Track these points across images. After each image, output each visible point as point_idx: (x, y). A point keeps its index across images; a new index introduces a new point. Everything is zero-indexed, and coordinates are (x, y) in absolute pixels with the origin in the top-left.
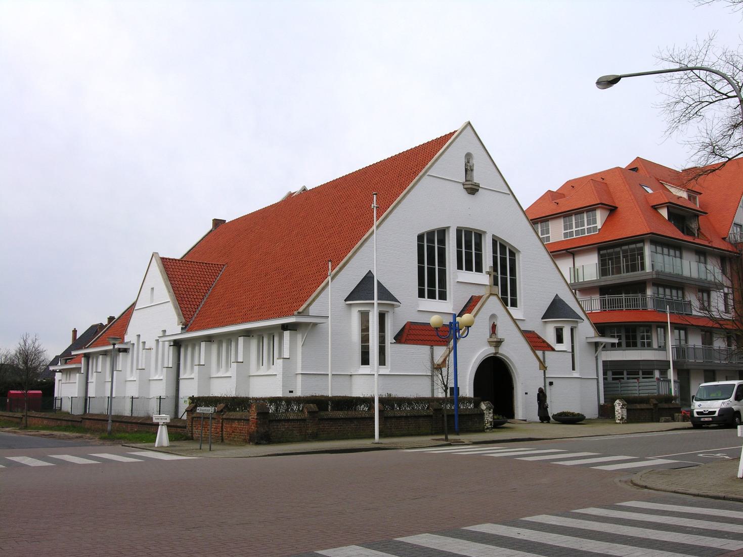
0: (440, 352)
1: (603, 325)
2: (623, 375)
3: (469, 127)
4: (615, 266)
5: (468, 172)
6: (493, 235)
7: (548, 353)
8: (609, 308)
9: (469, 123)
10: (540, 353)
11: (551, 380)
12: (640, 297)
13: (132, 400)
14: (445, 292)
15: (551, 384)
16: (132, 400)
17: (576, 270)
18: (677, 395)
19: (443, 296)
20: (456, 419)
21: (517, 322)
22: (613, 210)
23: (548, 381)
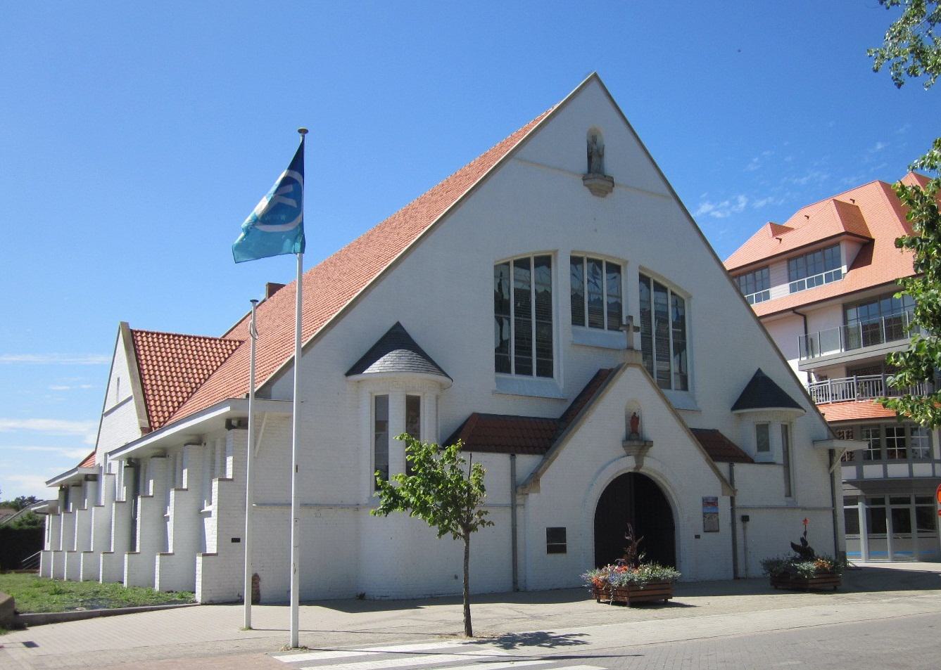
0: (526, 462)
1: (859, 423)
2: (893, 510)
3: (595, 83)
4: (869, 331)
5: (594, 159)
6: (640, 267)
7: (740, 469)
8: (833, 399)
9: (595, 75)
10: (723, 467)
11: (744, 513)
12: (854, 381)
13: (348, 506)
14: (551, 364)
15: (745, 519)
16: (348, 506)
17: (809, 341)
18: (21, 615)
19: (546, 370)
20: (247, 596)
21: (681, 413)
22: (868, 244)
23: (739, 514)
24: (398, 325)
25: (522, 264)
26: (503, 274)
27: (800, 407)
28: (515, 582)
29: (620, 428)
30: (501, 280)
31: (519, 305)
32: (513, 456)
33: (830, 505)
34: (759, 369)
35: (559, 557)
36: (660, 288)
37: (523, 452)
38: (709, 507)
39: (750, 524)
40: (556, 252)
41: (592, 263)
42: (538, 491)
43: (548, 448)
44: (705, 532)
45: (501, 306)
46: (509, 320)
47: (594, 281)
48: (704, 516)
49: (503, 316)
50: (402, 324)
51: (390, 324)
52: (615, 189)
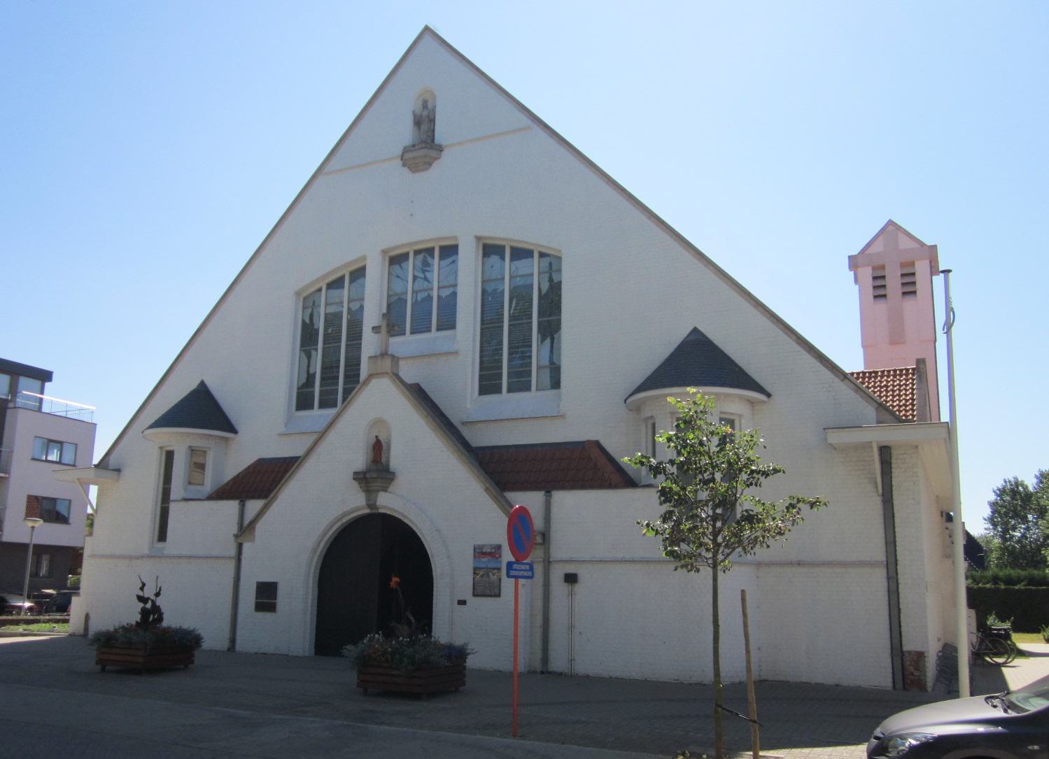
11: (571, 569)
15: (571, 579)
24: (695, 330)
25: (336, 284)
26: (316, 302)
27: (151, 427)
28: (233, 641)
29: (359, 460)
30: (313, 309)
31: (330, 331)
32: (548, 492)
33: (880, 555)
34: (202, 384)
35: (268, 616)
36: (520, 253)
37: (563, 487)
38: (484, 560)
39: (578, 588)
40: (478, 238)
41: (423, 254)
42: (253, 540)
43: (270, 491)
44: (474, 595)
45: (308, 335)
46: (316, 350)
47: (422, 276)
48: (474, 573)
49: (310, 348)
50: (700, 328)
51: (680, 334)
52: (400, 153)
